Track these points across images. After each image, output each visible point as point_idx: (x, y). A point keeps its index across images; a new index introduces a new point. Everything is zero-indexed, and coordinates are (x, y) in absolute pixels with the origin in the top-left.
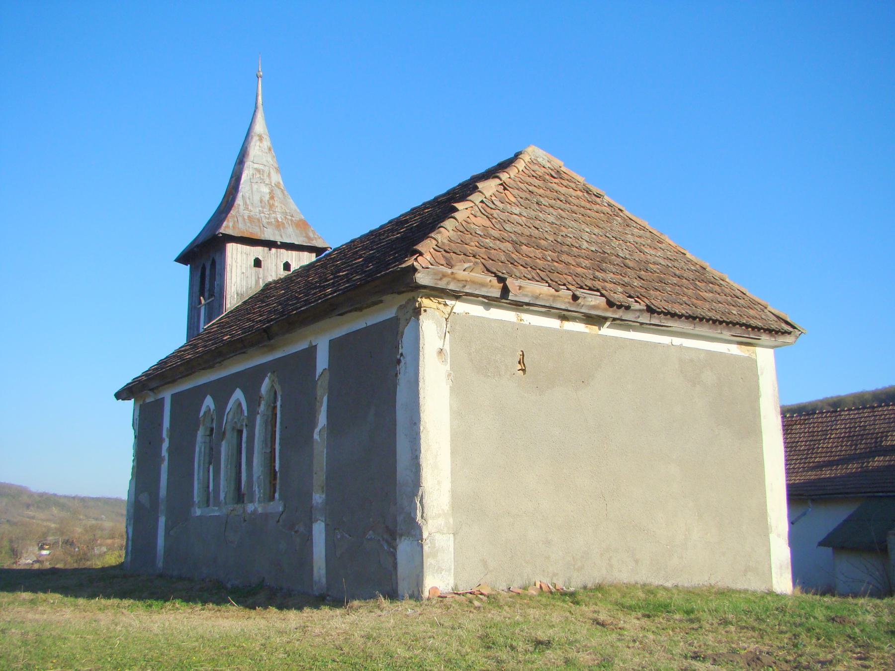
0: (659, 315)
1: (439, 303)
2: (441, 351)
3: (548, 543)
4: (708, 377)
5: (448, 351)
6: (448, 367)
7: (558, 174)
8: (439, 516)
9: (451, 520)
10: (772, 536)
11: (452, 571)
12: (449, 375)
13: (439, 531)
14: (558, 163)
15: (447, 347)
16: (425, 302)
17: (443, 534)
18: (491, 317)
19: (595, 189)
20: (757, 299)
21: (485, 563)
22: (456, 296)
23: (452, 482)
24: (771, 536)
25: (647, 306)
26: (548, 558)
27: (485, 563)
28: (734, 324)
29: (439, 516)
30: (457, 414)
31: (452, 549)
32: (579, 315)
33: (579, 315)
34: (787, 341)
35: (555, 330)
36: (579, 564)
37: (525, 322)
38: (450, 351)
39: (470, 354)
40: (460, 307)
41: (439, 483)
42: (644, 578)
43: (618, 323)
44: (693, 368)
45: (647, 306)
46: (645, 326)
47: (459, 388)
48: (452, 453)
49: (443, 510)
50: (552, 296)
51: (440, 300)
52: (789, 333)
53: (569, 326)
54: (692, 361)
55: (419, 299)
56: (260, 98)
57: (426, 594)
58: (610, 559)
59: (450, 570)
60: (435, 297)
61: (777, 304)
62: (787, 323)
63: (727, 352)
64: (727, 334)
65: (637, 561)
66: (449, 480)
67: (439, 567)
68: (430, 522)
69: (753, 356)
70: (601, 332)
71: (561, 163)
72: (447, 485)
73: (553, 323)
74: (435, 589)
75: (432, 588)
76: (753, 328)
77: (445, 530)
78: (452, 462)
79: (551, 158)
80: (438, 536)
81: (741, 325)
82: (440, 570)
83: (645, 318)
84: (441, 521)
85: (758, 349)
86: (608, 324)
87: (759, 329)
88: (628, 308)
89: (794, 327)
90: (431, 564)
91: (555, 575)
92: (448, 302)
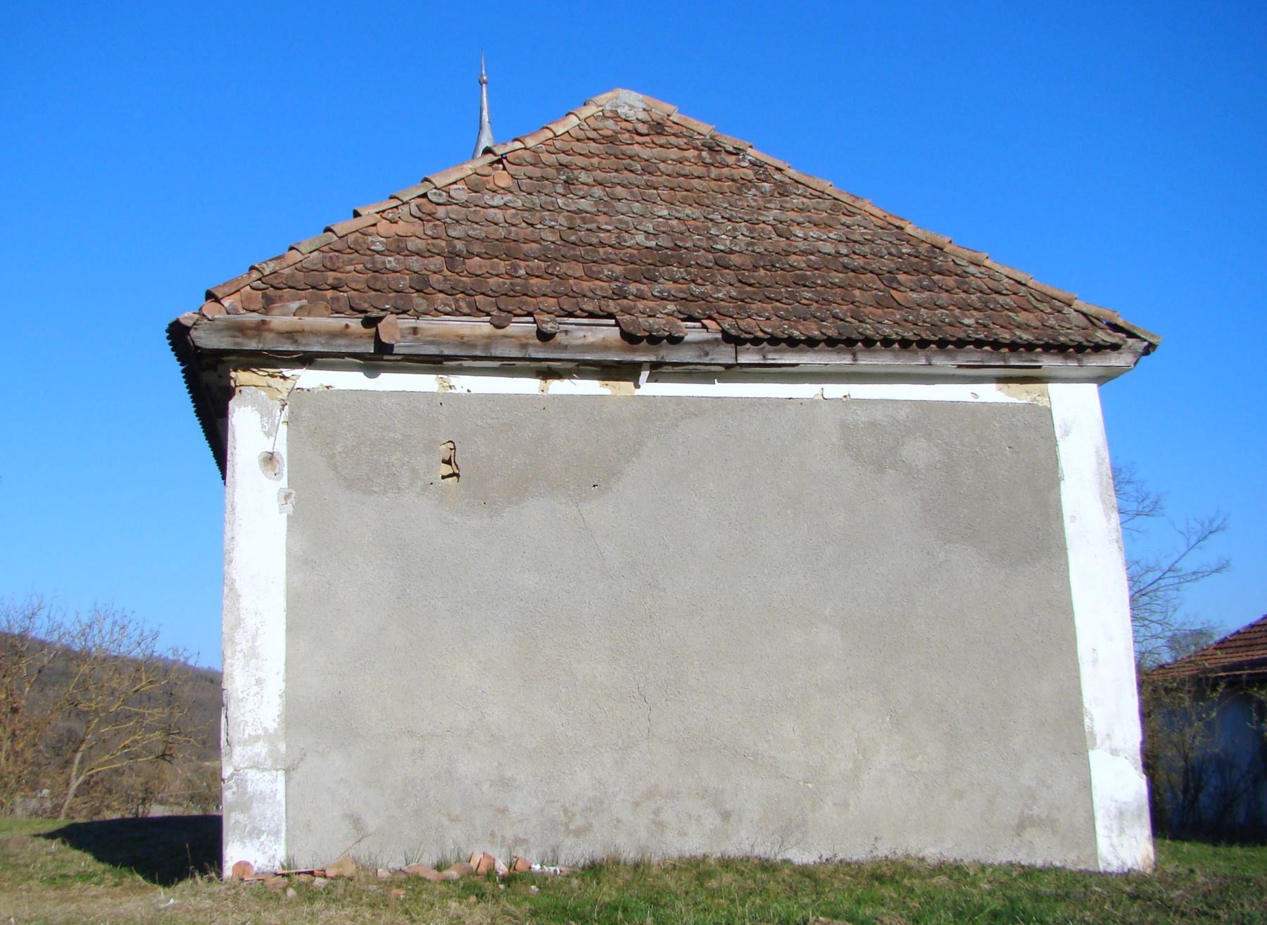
0: (754, 345)
1: (272, 376)
2: (270, 459)
3: (504, 783)
4: (918, 452)
5: (285, 456)
6: (284, 483)
7: (658, 128)
8: (256, 739)
9: (282, 747)
10: (1097, 758)
11: (283, 835)
12: (287, 497)
13: (257, 766)
14: (663, 109)
15: (282, 449)
16: (240, 377)
17: (264, 770)
18: (380, 388)
19: (729, 142)
20: (1049, 292)
21: (356, 821)
22: (307, 360)
23: (286, 680)
24: (1093, 755)
25: (723, 332)
26: (504, 810)
27: (356, 821)
28: (960, 344)
29: (256, 739)
30: (297, 562)
31: (281, 796)
32: (571, 365)
33: (571, 365)
34: (1113, 363)
35: (534, 397)
36: (578, 822)
37: (459, 390)
38: (290, 455)
39: (332, 457)
40: (308, 378)
41: (259, 682)
42: (748, 848)
43: (659, 371)
44: (874, 443)
45: (723, 332)
46: (664, 369)
47: (306, 514)
48: (289, 630)
49: (265, 729)
50: (489, 337)
51: (271, 371)
52: (1115, 347)
53: (559, 387)
54: (874, 424)
55: (233, 374)
56: (485, 113)
57: (228, 871)
58: (657, 812)
59: (277, 833)
60: (260, 366)
61: (1090, 295)
62: (1116, 328)
63: (970, 399)
64: (943, 363)
65: (726, 816)
66: (282, 675)
67: (254, 828)
68: (237, 750)
69: (1042, 402)
70: (637, 392)
71: (669, 108)
72: (276, 685)
73: (529, 386)
74: (243, 866)
75: (239, 864)
76: (1014, 347)
77: (269, 763)
78: (289, 646)
79: (653, 102)
80: (252, 775)
81: (979, 344)
82: (256, 833)
83: (725, 355)
84: (261, 749)
85: (1052, 388)
86: (645, 375)
87: (1030, 347)
88: (675, 340)
89: (1131, 335)
90: (238, 822)
91: (518, 841)
92: (287, 372)
